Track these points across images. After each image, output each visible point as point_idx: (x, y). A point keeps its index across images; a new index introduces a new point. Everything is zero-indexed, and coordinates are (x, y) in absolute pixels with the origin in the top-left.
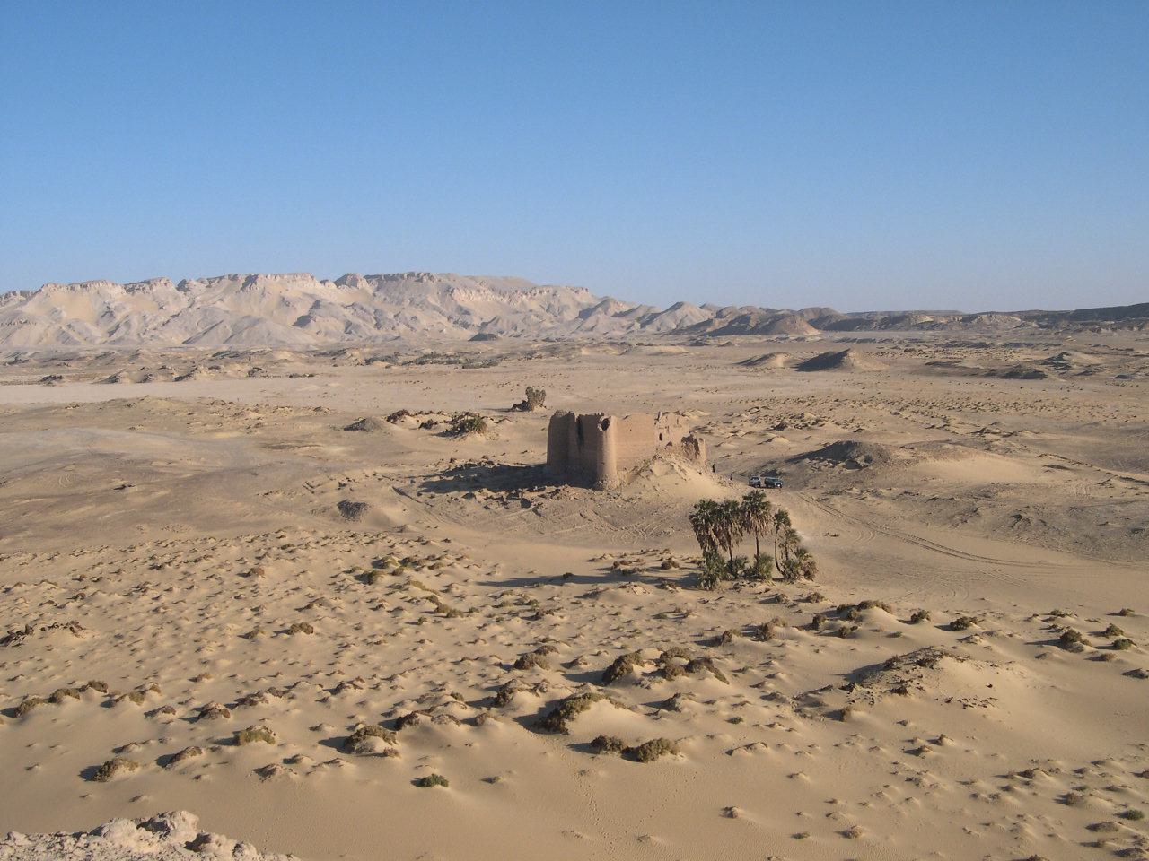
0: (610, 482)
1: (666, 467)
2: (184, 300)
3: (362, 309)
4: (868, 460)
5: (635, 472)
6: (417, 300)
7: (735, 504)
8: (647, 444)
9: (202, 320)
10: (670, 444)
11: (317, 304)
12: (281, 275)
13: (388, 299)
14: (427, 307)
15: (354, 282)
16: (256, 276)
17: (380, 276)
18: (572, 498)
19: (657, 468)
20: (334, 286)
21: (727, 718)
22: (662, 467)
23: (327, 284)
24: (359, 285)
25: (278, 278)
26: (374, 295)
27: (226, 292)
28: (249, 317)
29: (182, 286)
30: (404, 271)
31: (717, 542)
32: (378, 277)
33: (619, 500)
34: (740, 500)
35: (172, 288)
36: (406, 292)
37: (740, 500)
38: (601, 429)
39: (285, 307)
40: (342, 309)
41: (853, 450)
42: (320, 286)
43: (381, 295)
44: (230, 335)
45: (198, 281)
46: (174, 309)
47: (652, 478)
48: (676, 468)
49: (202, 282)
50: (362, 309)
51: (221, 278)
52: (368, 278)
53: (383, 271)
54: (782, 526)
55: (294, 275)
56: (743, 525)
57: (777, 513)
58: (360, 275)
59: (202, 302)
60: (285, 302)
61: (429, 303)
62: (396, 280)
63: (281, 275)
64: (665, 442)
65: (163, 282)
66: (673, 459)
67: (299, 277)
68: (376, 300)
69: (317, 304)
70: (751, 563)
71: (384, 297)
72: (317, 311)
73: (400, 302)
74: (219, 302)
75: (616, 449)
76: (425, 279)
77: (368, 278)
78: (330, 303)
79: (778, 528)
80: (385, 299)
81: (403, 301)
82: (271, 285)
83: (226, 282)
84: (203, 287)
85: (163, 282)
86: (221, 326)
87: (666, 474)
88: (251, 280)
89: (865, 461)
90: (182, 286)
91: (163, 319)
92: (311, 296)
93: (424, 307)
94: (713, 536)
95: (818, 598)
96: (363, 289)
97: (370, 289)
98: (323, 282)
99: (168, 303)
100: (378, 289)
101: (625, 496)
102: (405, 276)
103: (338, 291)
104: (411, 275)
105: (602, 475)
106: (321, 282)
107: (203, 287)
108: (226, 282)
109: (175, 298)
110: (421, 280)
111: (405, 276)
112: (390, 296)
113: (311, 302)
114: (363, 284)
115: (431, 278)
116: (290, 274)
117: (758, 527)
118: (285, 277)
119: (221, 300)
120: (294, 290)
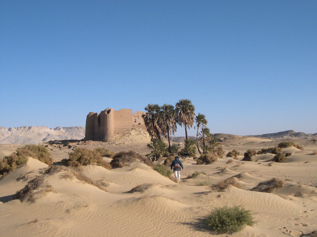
0: (110, 138)
1: (138, 132)
2: (10, 133)
3: (61, 136)
4: (225, 139)
5: (123, 134)
6: (77, 134)
7: (171, 107)
8: (129, 123)
9: (15, 139)
10: (139, 124)
11: (49, 135)
12: (38, 127)
13: (69, 134)
15: (59, 129)
16: (31, 127)
18: (92, 144)
20: (54, 130)
21: (190, 218)
23: (52, 129)
24: (61, 130)
25: (37, 128)
26: (65, 133)
27: (22, 131)
28: (28, 138)
29: (10, 129)
30: (74, 126)
31: (160, 131)
32: (66, 128)
35: (7, 130)
38: (106, 113)
39: (39, 136)
41: (218, 136)
42: (49, 130)
43: (67, 133)
44: (22, 143)
45: (14, 128)
46: (6, 136)
47: (130, 136)
48: (142, 132)
49: (15, 128)
50: (61, 136)
51: (21, 127)
53: (68, 126)
55: (42, 127)
56: (177, 121)
57: (197, 115)
58: (61, 127)
59: (15, 134)
60: (39, 134)
61: (81, 135)
62: (72, 129)
63: (38, 127)
64: (137, 123)
65: (4, 128)
67: (44, 127)
68: (66, 134)
69: (49, 135)
70: (182, 145)
71: (68, 133)
72: (48, 137)
73: (72, 135)
74: (20, 134)
75: (113, 124)
76: (80, 129)
78: (52, 135)
80: (68, 134)
81: (73, 134)
82: (35, 129)
83: (22, 128)
84: (16, 130)
85: (4, 128)
86: (20, 141)
87: (137, 135)
88: (30, 128)
89: (224, 139)
90: (10, 129)
91: (3, 138)
92: (47, 133)
94: (158, 127)
95: (236, 153)
96: (62, 131)
97: (64, 131)
98: (50, 129)
99: (5, 134)
100: (66, 131)
101: (117, 143)
102: (74, 128)
103: (55, 132)
104: (76, 127)
106: (50, 129)
107: (16, 130)
108: (22, 128)
109: (7, 133)
110: (78, 129)
113: (47, 134)
114: (62, 130)
115: (81, 128)
116: (41, 127)
118: (40, 127)
119: (21, 133)
120: (42, 131)
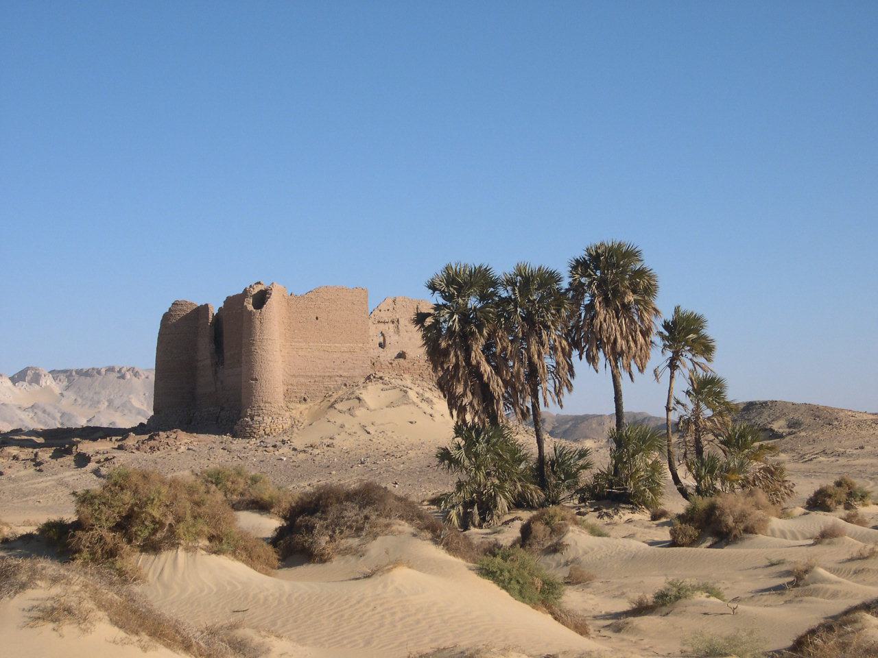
0: (268, 420)
1: (394, 395)
3: (44, 411)
6: (117, 402)
10: (402, 355)
13: (80, 400)
14: (130, 411)
15: (36, 379)
17: (71, 371)
18: (183, 448)
19: (372, 395)
20: (10, 383)
22: (383, 394)
24: (43, 382)
26: (62, 394)
30: (102, 365)
31: (497, 387)
33: (285, 449)
34: (563, 270)
36: (103, 392)
37: (563, 270)
38: (250, 307)
40: (18, 412)
43: (71, 396)
47: (360, 412)
48: (412, 394)
50: (44, 411)
52: (55, 373)
54: (686, 359)
58: (44, 370)
62: (91, 376)
64: (390, 353)
66: (408, 383)
68: (64, 401)
71: (73, 398)
76: (128, 376)
77: (55, 373)
79: (673, 366)
81: (98, 402)
87: (391, 405)
93: (126, 412)
94: (486, 368)
95: (851, 494)
96: (47, 387)
97: (56, 388)
100: (67, 388)
101: (298, 443)
102: (103, 371)
103: (16, 390)
105: (249, 404)
110: (123, 377)
111: (103, 371)
112: (82, 397)
114: (48, 381)
115: (136, 374)
117: (621, 343)
